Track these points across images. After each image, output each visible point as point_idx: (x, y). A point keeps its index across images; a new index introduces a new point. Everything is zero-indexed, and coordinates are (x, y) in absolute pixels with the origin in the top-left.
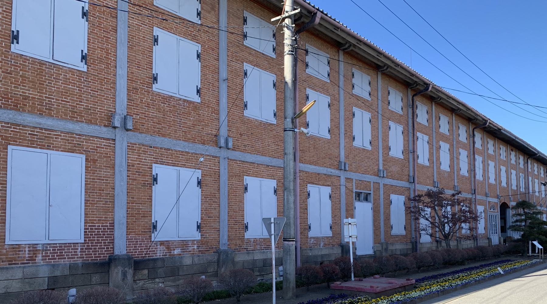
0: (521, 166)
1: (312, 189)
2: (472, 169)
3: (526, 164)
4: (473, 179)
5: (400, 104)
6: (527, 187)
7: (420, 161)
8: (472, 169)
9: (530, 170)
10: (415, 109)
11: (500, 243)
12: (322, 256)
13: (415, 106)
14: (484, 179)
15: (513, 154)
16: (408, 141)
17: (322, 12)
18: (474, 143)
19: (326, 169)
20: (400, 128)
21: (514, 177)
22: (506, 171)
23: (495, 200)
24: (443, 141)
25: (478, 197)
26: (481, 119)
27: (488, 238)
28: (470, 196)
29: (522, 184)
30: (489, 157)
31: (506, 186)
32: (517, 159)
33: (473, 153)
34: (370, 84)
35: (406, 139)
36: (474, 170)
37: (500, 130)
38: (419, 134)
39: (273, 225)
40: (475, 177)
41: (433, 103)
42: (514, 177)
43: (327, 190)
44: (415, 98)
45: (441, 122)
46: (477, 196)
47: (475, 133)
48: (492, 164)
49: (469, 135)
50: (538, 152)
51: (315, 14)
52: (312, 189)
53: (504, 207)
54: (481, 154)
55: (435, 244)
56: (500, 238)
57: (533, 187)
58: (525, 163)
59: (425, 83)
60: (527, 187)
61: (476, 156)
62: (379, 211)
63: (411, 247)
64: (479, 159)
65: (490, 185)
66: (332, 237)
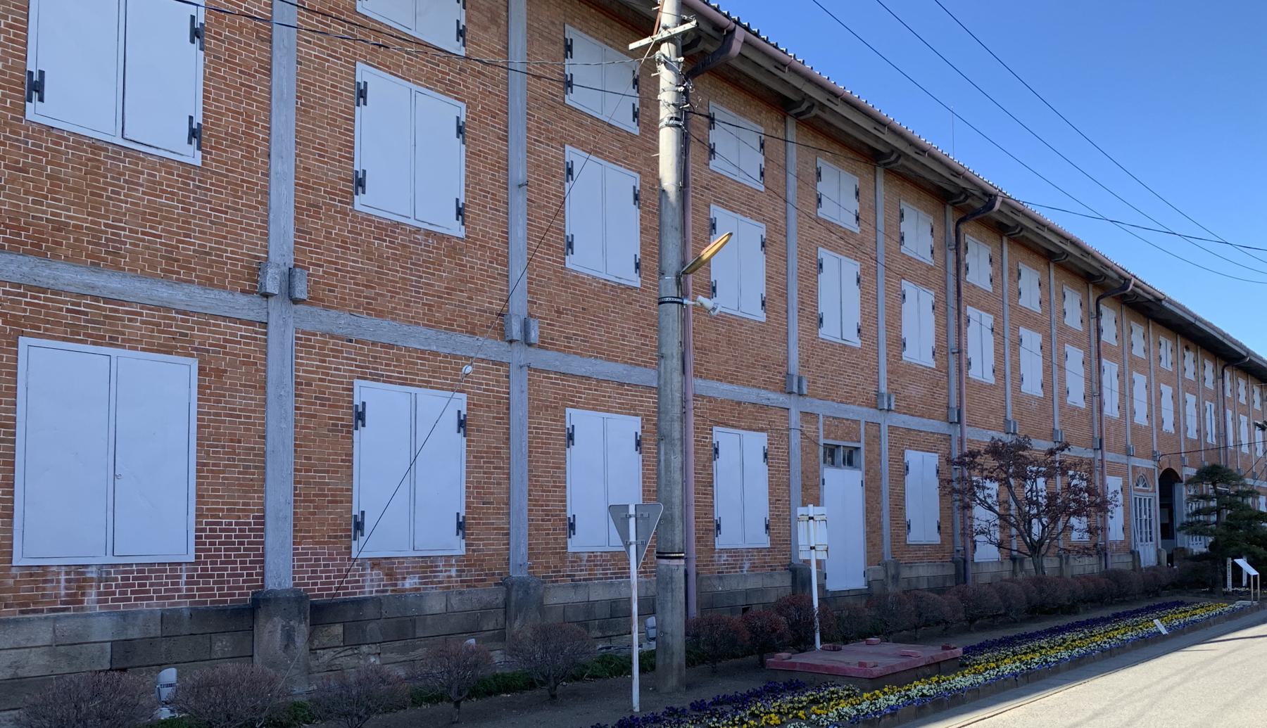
0: (1209, 384)
1: (723, 437)
2: (1095, 393)
3: (1220, 381)
4: (1096, 415)
5: (928, 241)
6: (1221, 434)
7: (974, 373)
8: (1095, 393)
9: (1228, 394)
10: (962, 253)
11: (1159, 563)
12: (747, 593)
13: (963, 247)
14: (1123, 415)
15: (1190, 356)
16: (946, 326)
17: (747, 29)
18: (1099, 331)
19: (755, 390)
20: (928, 298)
21: (1191, 410)
22: (1174, 397)
23: (1148, 464)
24: (1028, 327)
25: (1109, 456)
26: (1116, 276)
27: (1132, 552)
28: (1089, 454)
29: (1211, 427)
30: (1135, 363)
31: (1172, 430)
32: (1200, 367)
33: (1096, 355)
34: (857, 194)
35: (942, 322)
36: (1100, 395)
37: (1160, 300)
38: (971, 312)
39: (632, 521)
40: (1101, 410)
41: (1005, 239)
42: (1191, 410)
43: (757, 441)
44: (961, 227)
45: (1023, 284)
46: (967, 429)
47: (1102, 307)
48: (1140, 380)
49: (1087, 313)
50: (1248, 352)
51: (732, 32)
52: (723, 437)
53: (1169, 480)
54: (1115, 356)
55: (1008, 565)
56: (1158, 551)
57: (1237, 433)
58: (1217, 377)
59: (986, 193)
60: (1221, 434)
61: (1104, 362)
62: (879, 488)
63: (952, 572)
64: (1110, 369)
65: (1136, 428)
66: (769, 550)
